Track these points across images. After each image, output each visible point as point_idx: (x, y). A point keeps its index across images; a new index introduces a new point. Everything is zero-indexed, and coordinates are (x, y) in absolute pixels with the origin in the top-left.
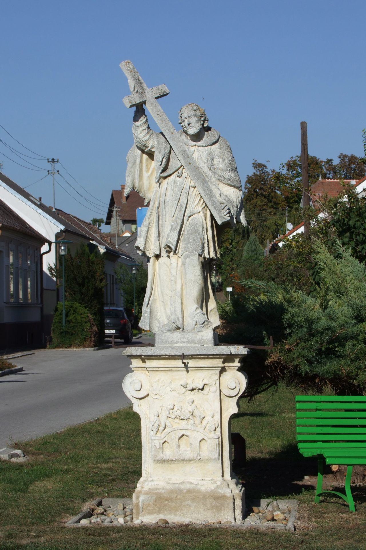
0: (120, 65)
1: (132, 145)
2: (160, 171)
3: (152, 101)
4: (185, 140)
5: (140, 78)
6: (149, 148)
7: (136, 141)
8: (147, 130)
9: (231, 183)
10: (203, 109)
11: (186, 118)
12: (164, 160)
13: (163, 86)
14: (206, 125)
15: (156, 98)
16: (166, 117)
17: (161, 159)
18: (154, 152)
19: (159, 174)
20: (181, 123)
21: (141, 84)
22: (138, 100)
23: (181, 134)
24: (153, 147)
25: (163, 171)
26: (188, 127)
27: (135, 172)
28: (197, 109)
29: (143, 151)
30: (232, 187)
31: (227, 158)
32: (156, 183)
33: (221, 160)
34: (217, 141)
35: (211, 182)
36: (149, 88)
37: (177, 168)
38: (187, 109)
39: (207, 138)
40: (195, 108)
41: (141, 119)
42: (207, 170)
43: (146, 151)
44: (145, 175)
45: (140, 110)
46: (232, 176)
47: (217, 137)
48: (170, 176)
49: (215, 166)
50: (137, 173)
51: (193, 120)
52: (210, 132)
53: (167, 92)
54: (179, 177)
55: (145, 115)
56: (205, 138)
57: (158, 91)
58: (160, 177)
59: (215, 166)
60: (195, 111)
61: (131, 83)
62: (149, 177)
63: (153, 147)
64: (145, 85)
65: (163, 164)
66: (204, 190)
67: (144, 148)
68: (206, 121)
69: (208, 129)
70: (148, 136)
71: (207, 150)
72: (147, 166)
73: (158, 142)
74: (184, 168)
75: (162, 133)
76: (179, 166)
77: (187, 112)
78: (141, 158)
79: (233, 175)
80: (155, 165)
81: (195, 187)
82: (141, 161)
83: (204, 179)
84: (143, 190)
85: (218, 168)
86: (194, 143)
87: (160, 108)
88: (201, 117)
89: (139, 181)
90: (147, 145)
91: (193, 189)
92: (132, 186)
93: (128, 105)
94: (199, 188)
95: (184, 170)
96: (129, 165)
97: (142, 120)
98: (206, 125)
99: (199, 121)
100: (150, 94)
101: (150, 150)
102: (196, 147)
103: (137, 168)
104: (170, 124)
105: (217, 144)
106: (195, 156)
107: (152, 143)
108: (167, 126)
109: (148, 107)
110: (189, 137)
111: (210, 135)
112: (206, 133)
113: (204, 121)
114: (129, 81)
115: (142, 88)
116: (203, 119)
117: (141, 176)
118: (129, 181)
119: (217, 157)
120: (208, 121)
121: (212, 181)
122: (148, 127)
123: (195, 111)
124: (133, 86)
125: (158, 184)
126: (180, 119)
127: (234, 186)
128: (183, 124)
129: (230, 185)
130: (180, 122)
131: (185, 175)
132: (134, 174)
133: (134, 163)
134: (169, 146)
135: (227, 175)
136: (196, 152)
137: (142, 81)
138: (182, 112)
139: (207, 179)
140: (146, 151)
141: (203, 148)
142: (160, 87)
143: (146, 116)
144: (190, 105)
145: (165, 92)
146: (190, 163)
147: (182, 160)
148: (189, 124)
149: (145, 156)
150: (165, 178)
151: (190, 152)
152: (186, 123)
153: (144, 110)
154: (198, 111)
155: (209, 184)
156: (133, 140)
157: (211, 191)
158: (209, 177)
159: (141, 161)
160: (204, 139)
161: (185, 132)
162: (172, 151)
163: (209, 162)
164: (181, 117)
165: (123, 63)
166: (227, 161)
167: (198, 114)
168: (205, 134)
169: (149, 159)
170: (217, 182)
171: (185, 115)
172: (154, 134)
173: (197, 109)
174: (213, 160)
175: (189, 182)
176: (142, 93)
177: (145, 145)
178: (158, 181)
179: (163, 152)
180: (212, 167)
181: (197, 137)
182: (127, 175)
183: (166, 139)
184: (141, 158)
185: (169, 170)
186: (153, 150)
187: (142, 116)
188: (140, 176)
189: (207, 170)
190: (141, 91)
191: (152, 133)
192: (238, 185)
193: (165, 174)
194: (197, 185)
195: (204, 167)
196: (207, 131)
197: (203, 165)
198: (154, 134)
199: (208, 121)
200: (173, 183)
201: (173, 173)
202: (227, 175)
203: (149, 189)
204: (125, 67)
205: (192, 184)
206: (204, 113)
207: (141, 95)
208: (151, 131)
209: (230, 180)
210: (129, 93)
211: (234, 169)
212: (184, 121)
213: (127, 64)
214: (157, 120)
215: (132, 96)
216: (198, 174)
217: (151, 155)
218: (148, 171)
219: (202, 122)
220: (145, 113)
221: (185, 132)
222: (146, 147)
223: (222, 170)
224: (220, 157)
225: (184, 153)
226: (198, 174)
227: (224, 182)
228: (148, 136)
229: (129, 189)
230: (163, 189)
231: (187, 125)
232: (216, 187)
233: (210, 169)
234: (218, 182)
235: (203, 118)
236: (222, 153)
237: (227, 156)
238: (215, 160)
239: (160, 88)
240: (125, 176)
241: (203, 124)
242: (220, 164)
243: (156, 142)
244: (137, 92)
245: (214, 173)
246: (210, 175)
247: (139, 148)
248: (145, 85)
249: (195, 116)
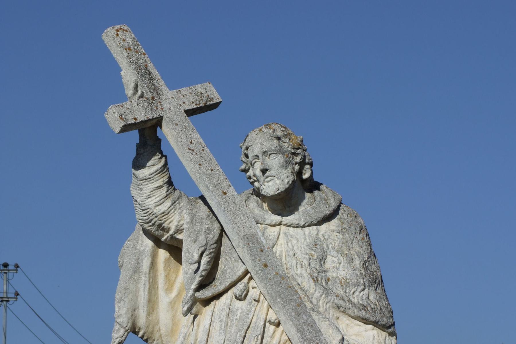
0: (104, 37)
1: (132, 230)
2: (194, 286)
3: (176, 120)
4: (257, 211)
5: (151, 66)
6: (171, 232)
7: (139, 215)
8: (165, 189)
9: (368, 316)
10: (300, 137)
11: (257, 157)
12: (205, 260)
13: (207, 85)
14: (306, 176)
15: (190, 113)
16: (212, 157)
17: (196, 257)
18: (181, 241)
19: (191, 292)
20: (246, 171)
21: (151, 78)
22: (142, 114)
23: (248, 198)
24: (179, 230)
25: (201, 286)
26: (262, 179)
27: (137, 291)
28: (285, 136)
29: (158, 242)
30: (370, 327)
31: (359, 254)
32: (185, 315)
33: (343, 260)
34: (334, 214)
35: (318, 312)
36: (171, 88)
37: (235, 278)
38: (261, 134)
39: (309, 206)
40: (279, 133)
41: (150, 163)
42: (308, 284)
43: (163, 239)
44: (164, 300)
45: (148, 138)
46: (372, 297)
47: (333, 204)
48: (218, 296)
49: (329, 275)
50: (141, 293)
51: (275, 162)
52: (316, 192)
53: (217, 101)
54: (239, 298)
55: (161, 152)
56: (305, 207)
57: (192, 98)
58: (195, 301)
59: (329, 275)
60: (279, 139)
61: (129, 76)
62: (172, 304)
63: (179, 230)
64: (160, 83)
65: (202, 268)
66: (300, 331)
67: (160, 233)
68: (308, 166)
69: (313, 186)
70: (168, 203)
71: (310, 236)
72: (167, 276)
73: (193, 218)
74: (251, 278)
75: (203, 198)
76: (240, 273)
77: (259, 141)
78: (154, 257)
79: (372, 297)
80: (184, 277)
81: (278, 325)
82: (153, 266)
83: (301, 304)
84: (156, 336)
85: (335, 279)
86: (277, 218)
87: (197, 135)
88: (294, 154)
89: (149, 314)
90: (165, 225)
91: (272, 328)
92: (129, 325)
93: (117, 126)
94: (288, 327)
95: (252, 283)
96: (124, 274)
97: (155, 164)
98: (306, 176)
99: (286, 165)
100: (173, 103)
101: (172, 236)
102: (283, 228)
103: (143, 281)
104: (220, 173)
105: (335, 222)
106: (280, 248)
107: (178, 219)
108: (210, 177)
109: (168, 132)
110: (265, 205)
111: (318, 199)
112: (307, 195)
113: (302, 164)
114: (122, 73)
115: (155, 89)
116: (298, 159)
117: (152, 302)
118: (123, 311)
119: (334, 253)
120: (311, 164)
121: (321, 310)
122: (170, 183)
123: (279, 139)
124: (132, 85)
125: (191, 317)
126: (244, 159)
127: (375, 324)
128: (250, 173)
129: (366, 321)
130: (243, 167)
131: (253, 293)
132: (136, 296)
133: (137, 269)
134: (216, 226)
135: (358, 296)
136: (281, 241)
137: (155, 72)
138: (247, 143)
139: (309, 305)
140: (163, 239)
141: (299, 230)
142: (199, 87)
143: (163, 156)
144: (268, 126)
145: (211, 99)
146: (266, 266)
147: (247, 259)
148: (264, 171)
149: (163, 254)
150: (207, 302)
151: (267, 239)
152: (258, 166)
153: (158, 141)
154: (287, 140)
155: (314, 316)
156: (134, 215)
157: (318, 332)
158: (314, 300)
159: (153, 266)
160: (301, 209)
161: (257, 193)
162: (225, 240)
163: (313, 265)
164: (247, 156)
165: (110, 31)
166: (357, 262)
167: (287, 146)
168: (304, 198)
169: (173, 261)
170: (333, 313)
171: (255, 150)
172: (184, 198)
173: (285, 136)
174: (323, 259)
175: (262, 312)
176: (153, 98)
177: (160, 225)
178: (189, 310)
179: (202, 239)
180: (320, 277)
181: (284, 203)
182: (117, 296)
183: (210, 208)
184: (154, 257)
185: (216, 283)
186: (179, 237)
187: (154, 155)
188: (149, 301)
189: (308, 284)
190: (150, 95)
191: (180, 197)
192: (385, 320)
193: (207, 293)
194: (282, 319)
195: (301, 276)
196: (311, 191)
197: (299, 271)
198: (184, 198)
199: (311, 164)
200: (224, 313)
201: (225, 291)
202: (358, 296)
203: (173, 332)
204: (117, 41)
205: (272, 316)
206: (300, 146)
207: (150, 104)
208: (177, 193)
209: (365, 308)
210: (119, 96)
211: (376, 282)
212: (253, 165)
213: (120, 33)
214: (188, 163)
215: (127, 104)
216: (285, 291)
217: (175, 249)
218: (169, 289)
219: (297, 167)
220: (162, 148)
221: (257, 193)
222: (164, 229)
223: (345, 284)
224: (342, 253)
225: (251, 239)
226: (285, 291)
227: (350, 312)
228: (168, 203)
229: (122, 331)
230: (201, 328)
231: (258, 173)
232: (331, 324)
233: (316, 281)
234: (337, 314)
235: (299, 157)
236: (345, 242)
237: (359, 249)
238: (329, 259)
239: (200, 90)
240: (114, 300)
241: (299, 173)
242: (340, 269)
243: (187, 218)
244: (142, 96)
245: (327, 291)
246: (317, 294)
247: (147, 233)
248: (162, 82)
249: (280, 151)
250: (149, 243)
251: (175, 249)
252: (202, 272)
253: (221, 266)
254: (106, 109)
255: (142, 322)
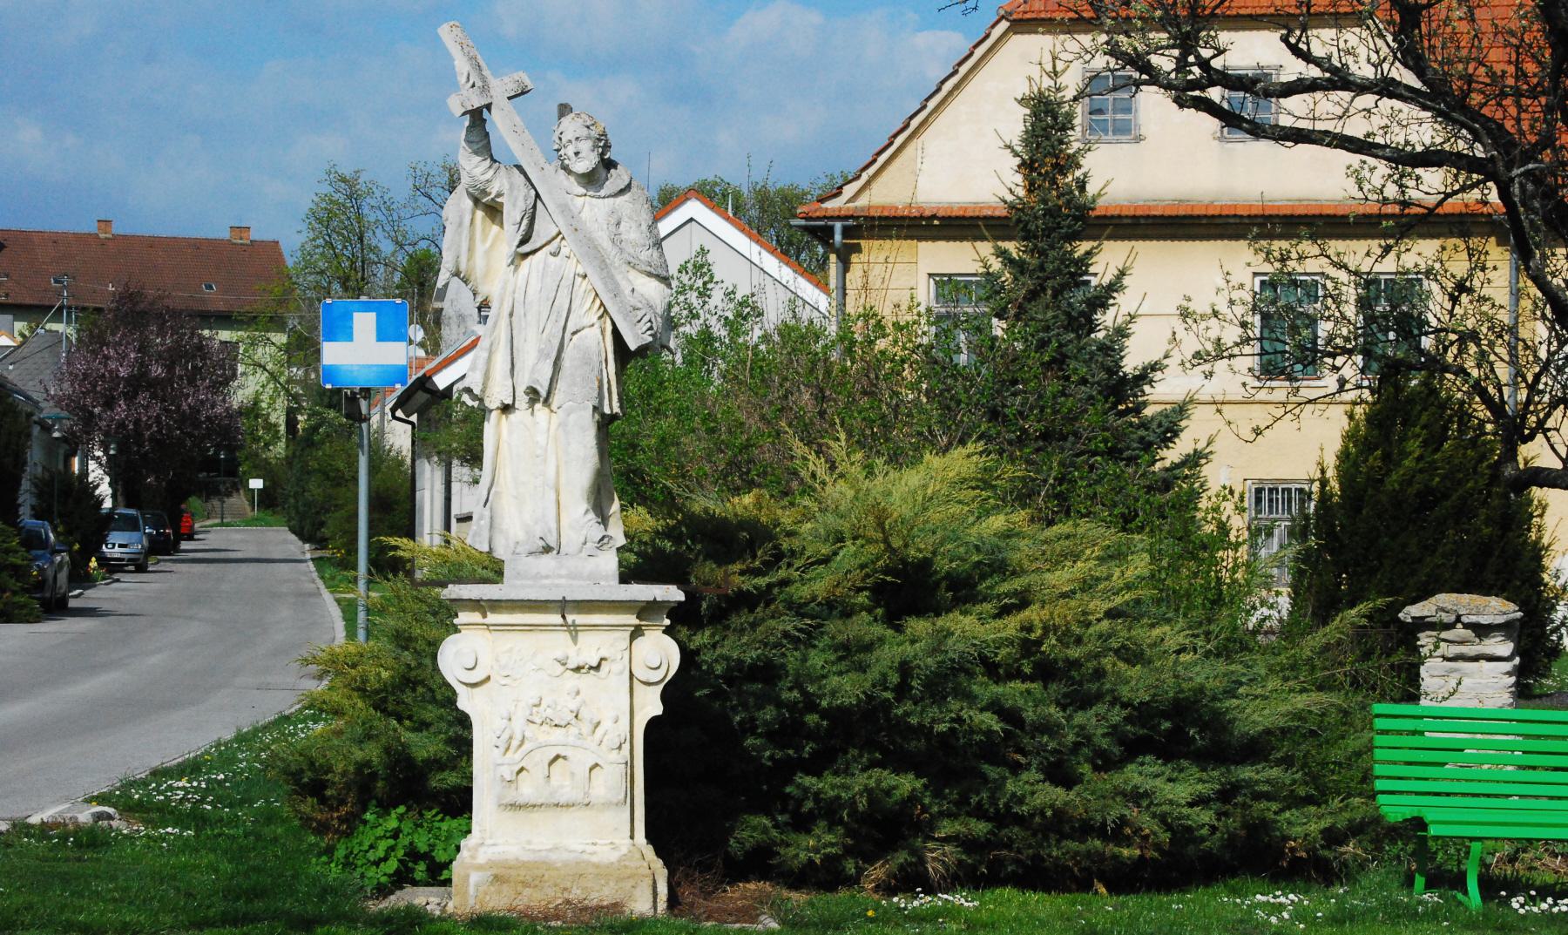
0: (439, 31)
2: (516, 243)
4: (565, 183)
12: (525, 222)
22: (477, 102)
25: (523, 242)
29: (476, 201)
33: (634, 225)
34: (628, 188)
49: (623, 237)
51: (585, 146)
54: (554, 254)
61: (462, 66)
63: (499, 195)
64: (486, 72)
70: (491, 172)
75: (519, 167)
80: (505, 238)
81: (585, 276)
82: (472, 220)
93: (458, 111)
99: (595, 147)
100: (500, 88)
103: (465, 232)
105: (627, 197)
106: (585, 215)
107: (502, 184)
115: (484, 79)
117: (471, 250)
129: (650, 274)
131: (565, 251)
133: (460, 224)
134: (533, 193)
136: (587, 208)
137: (482, 64)
148: (577, 154)
149: (480, 214)
150: (525, 255)
159: (472, 220)
161: (566, 168)
170: (625, 267)
180: (616, 240)
193: (526, 248)
202: (645, 255)
205: (580, 270)
210: (455, 87)
217: (494, 211)
218: (484, 240)
221: (566, 168)
225: (565, 209)
228: (491, 172)
243: (507, 186)
247: (469, 194)
250: (469, 203)
251: (494, 211)
252: (521, 232)
253: (536, 227)
254: (448, 96)
255: (463, 267)
